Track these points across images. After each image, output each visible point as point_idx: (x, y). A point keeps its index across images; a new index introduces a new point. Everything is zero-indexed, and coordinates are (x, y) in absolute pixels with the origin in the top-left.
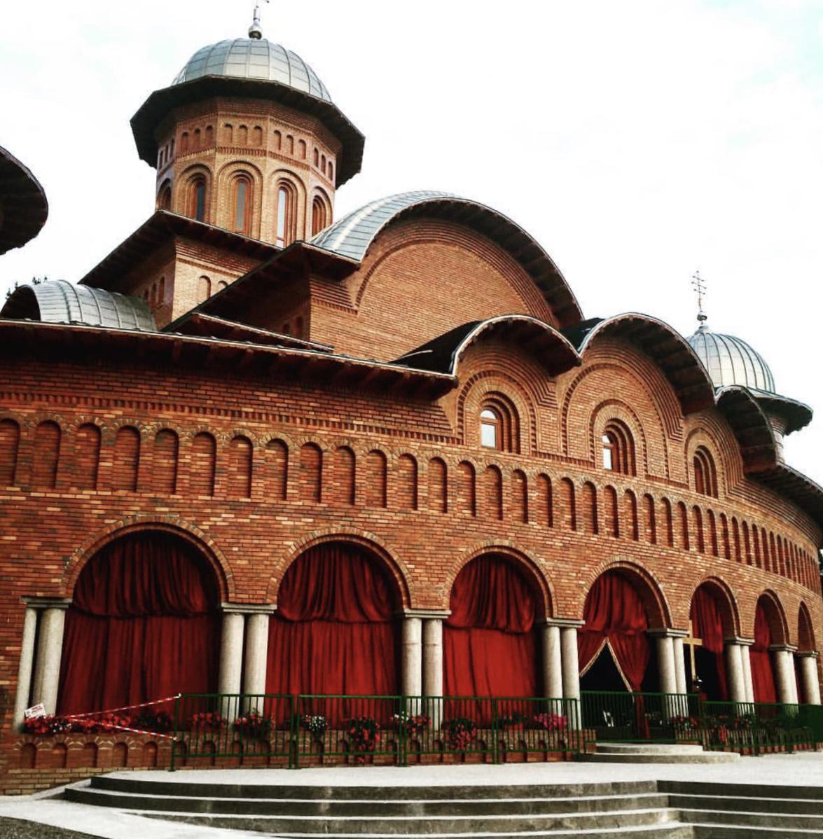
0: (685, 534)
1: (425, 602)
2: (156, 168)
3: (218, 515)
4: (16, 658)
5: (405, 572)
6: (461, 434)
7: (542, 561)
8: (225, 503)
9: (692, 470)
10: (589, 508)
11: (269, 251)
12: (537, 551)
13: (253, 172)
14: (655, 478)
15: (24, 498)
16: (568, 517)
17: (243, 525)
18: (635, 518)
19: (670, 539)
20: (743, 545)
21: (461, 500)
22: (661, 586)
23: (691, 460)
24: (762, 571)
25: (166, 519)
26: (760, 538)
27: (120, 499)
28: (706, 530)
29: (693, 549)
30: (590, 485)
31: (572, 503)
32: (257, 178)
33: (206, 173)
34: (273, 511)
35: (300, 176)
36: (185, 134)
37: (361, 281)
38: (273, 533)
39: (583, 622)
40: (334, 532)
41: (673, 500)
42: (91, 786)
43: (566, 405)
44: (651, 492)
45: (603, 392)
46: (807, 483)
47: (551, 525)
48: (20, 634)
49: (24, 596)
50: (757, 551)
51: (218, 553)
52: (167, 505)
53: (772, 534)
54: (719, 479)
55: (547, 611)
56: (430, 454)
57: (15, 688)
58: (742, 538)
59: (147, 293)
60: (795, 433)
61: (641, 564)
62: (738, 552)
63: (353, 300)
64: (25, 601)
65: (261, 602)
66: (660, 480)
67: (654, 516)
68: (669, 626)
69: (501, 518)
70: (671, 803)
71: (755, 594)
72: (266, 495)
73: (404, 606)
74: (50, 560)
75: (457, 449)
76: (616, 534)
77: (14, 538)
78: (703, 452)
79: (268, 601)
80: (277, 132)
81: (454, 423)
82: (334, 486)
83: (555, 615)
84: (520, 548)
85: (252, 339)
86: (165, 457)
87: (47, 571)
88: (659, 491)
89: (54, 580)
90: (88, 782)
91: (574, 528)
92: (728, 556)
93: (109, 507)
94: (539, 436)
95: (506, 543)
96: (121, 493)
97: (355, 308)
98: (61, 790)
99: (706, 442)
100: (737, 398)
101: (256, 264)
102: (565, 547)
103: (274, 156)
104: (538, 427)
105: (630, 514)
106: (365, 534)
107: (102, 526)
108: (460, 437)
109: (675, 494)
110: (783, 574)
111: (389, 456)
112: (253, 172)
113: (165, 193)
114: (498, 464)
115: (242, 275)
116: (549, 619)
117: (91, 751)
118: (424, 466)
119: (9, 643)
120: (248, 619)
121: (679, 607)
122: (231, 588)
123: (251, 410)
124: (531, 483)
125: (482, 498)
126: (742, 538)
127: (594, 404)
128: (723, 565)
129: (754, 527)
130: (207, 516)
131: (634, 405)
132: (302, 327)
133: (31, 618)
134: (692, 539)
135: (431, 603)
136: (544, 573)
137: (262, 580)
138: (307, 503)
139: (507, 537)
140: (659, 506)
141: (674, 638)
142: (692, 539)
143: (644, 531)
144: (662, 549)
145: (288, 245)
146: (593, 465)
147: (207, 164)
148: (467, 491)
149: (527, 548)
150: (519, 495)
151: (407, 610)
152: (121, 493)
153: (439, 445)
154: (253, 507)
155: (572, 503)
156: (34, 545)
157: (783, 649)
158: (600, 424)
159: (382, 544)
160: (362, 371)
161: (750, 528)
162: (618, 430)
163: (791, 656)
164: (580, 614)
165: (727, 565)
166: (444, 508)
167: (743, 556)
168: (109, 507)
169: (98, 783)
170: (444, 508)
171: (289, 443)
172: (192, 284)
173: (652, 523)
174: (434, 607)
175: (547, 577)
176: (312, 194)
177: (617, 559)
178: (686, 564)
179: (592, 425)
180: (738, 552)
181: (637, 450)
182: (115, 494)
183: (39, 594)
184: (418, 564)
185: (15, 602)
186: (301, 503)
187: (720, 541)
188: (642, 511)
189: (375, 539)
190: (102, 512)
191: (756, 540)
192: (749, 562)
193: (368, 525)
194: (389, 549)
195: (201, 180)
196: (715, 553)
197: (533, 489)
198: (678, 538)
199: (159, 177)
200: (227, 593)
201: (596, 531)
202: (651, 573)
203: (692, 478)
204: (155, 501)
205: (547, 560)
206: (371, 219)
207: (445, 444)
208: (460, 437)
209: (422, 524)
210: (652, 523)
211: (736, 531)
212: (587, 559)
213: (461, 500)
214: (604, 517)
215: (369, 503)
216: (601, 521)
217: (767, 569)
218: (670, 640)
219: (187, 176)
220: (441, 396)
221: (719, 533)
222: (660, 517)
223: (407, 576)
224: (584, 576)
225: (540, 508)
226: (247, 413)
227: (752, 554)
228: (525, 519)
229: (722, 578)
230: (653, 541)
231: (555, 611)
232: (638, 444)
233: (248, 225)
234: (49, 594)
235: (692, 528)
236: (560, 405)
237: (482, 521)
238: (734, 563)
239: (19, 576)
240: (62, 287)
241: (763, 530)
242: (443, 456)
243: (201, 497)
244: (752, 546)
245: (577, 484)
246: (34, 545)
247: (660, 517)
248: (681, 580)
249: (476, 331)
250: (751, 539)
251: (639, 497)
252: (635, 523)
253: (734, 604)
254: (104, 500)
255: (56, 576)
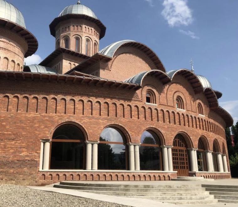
0: (196, 125)
1: (135, 141)
2: (55, 37)
3: (85, 119)
4: (39, 153)
5: (129, 133)
6: (142, 100)
7: (162, 131)
8: (86, 116)
9: (197, 109)
10: (174, 118)
11: (84, 57)
12: (161, 129)
13: (80, 37)
14: (189, 110)
15: (40, 116)
16: (168, 120)
17: (91, 122)
18: (184, 121)
19: (193, 126)
20: (209, 127)
21: (142, 116)
22: (191, 137)
23: (197, 106)
24: (214, 134)
25: (73, 120)
26: (213, 126)
27: (62, 116)
28: (201, 123)
29: (198, 128)
30: (173, 112)
31: (169, 117)
32: (81, 39)
33: (68, 37)
34: (98, 119)
35: (91, 38)
36: (63, 28)
37: (111, 64)
38: (98, 124)
39: (173, 146)
40: (112, 123)
41: (193, 116)
42: (60, 184)
43: (167, 92)
44: (188, 114)
45: (174, 90)
46: (225, 112)
47: (164, 122)
48: (40, 148)
49: (41, 139)
50: (213, 129)
51: (85, 129)
52: (73, 117)
53: (216, 125)
54: (204, 111)
55: (164, 143)
56: (135, 105)
57: (39, 161)
58: (209, 126)
59: (55, 67)
60: (219, 98)
61: (186, 132)
62: (208, 129)
63: (110, 67)
64: (41, 140)
65: (96, 141)
66: (190, 111)
67: (186, 119)
68: (193, 147)
69: (152, 120)
70: (207, 190)
71: (213, 139)
72: (96, 115)
73: (130, 142)
74: (46, 130)
75: (141, 103)
76: (180, 125)
77: (38, 125)
78: (199, 104)
79: (98, 140)
80: (85, 27)
81: (140, 96)
82: (112, 112)
83: (166, 145)
84: (157, 128)
85: (85, 76)
86: (72, 105)
87: (45, 133)
88: (190, 114)
89: (48, 135)
90: (59, 183)
91: (170, 123)
92: (206, 130)
93: (60, 118)
94: (161, 100)
95: (154, 127)
96: (62, 114)
97: (110, 69)
98: (53, 185)
99: (201, 102)
100: (208, 90)
101: (84, 61)
102: (168, 128)
103: (84, 32)
104: (160, 98)
105: (183, 119)
106: (120, 124)
107: (58, 122)
108: (141, 100)
109: (194, 114)
110: (219, 135)
111: (124, 105)
112: (80, 37)
113: (58, 43)
114: (151, 107)
115: (81, 63)
116: (164, 146)
117: (58, 176)
118: (133, 108)
119: (37, 150)
120: (92, 144)
121: (196, 143)
122: (89, 137)
123: (92, 94)
124: (159, 112)
125: (147, 115)
126: (209, 126)
127: (173, 92)
128: (205, 132)
129: (212, 123)
130: (82, 120)
131: (183, 92)
132: (98, 74)
133: (42, 144)
134: (198, 126)
135: (136, 141)
136: (163, 134)
137: (96, 135)
138: (106, 116)
139: (154, 125)
140: (190, 117)
141: (194, 151)
142: (198, 126)
143: (187, 124)
144: (191, 128)
145: (93, 55)
146: (174, 107)
147: (68, 35)
148: (144, 114)
149: (159, 128)
150: (156, 115)
151: (130, 143)
152: (62, 114)
153: (137, 102)
154: (93, 118)
155: (169, 117)
156: (43, 127)
157: (219, 154)
158: (175, 97)
159: (124, 127)
160: (119, 84)
161: (211, 123)
162: (179, 99)
163: (221, 155)
164: (172, 144)
165: (206, 132)
166: (138, 118)
167: (210, 130)
168: (60, 118)
169: (61, 183)
170: (138, 118)
171: (101, 102)
172: (67, 66)
173: (188, 122)
174: (137, 142)
175: (164, 135)
176: (94, 42)
177: (181, 131)
178: (197, 132)
179: (173, 97)
180: (208, 129)
181: (184, 103)
182: (61, 114)
183: (44, 139)
184: (133, 132)
185: (39, 140)
186: (104, 117)
187: (204, 126)
188: (186, 119)
189: (122, 125)
190: (58, 119)
191: (212, 126)
192: (211, 132)
193: (121, 122)
194: (126, 128)
195: (67, 40)
196: (203, 129)
197: (160, 113)
198: (195, 126)
199: (56, 39)
200: (88, 138)
201: (175, 124)
202: (189, 134)
203: (197, 110)
204: (70, 116)
205: (164, 131)
206: (114, 47)
207: (138, 102)
208: (141, 100)
209: (133, 122)
210: (188, 122)
211: (208, 124)
212: (173, 131)
213: (142, 116)
214: (177, 121)
215: (120, 117)
216: (176, 121)
217: (215, 133)
218: (193, 151)
219: (63, 39)
220: (137, 90)
221: (204, 124)
222: (190, 120)
223: (130, 135)
224: (172, 135)
225: (161, 118)
226: (91, 95)
227: (212, 130)
228: (158, 121)
229: (205, 135)
230: (189, 126)
231: (166, 143)
232: (185, 102)
233: (79, 50)
234: (47, 139)
235: (198, 123)
236: (166, 92)
237: (148, 121)
238: (208, 132)
239: (39, 134)
240: (35, 65)
241: (214, 124)
242: (137, 105)
243: (81, 115)
244: (212, 128)
245: (170, 112)
246: (43, 127)
247: (190, 120)
248: (196, 136)
249: (146, 74)
250: (211, 126)
251: (185, 115)
252: (184, 122)
253: (208, 142)
254: (58, 116)
255: (48, 134)
